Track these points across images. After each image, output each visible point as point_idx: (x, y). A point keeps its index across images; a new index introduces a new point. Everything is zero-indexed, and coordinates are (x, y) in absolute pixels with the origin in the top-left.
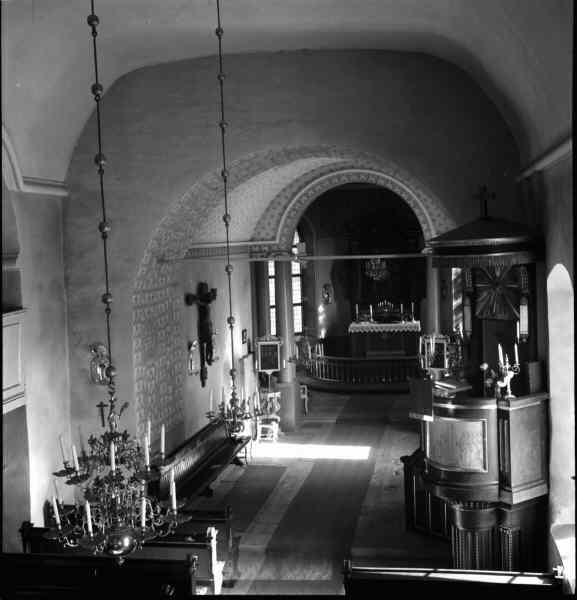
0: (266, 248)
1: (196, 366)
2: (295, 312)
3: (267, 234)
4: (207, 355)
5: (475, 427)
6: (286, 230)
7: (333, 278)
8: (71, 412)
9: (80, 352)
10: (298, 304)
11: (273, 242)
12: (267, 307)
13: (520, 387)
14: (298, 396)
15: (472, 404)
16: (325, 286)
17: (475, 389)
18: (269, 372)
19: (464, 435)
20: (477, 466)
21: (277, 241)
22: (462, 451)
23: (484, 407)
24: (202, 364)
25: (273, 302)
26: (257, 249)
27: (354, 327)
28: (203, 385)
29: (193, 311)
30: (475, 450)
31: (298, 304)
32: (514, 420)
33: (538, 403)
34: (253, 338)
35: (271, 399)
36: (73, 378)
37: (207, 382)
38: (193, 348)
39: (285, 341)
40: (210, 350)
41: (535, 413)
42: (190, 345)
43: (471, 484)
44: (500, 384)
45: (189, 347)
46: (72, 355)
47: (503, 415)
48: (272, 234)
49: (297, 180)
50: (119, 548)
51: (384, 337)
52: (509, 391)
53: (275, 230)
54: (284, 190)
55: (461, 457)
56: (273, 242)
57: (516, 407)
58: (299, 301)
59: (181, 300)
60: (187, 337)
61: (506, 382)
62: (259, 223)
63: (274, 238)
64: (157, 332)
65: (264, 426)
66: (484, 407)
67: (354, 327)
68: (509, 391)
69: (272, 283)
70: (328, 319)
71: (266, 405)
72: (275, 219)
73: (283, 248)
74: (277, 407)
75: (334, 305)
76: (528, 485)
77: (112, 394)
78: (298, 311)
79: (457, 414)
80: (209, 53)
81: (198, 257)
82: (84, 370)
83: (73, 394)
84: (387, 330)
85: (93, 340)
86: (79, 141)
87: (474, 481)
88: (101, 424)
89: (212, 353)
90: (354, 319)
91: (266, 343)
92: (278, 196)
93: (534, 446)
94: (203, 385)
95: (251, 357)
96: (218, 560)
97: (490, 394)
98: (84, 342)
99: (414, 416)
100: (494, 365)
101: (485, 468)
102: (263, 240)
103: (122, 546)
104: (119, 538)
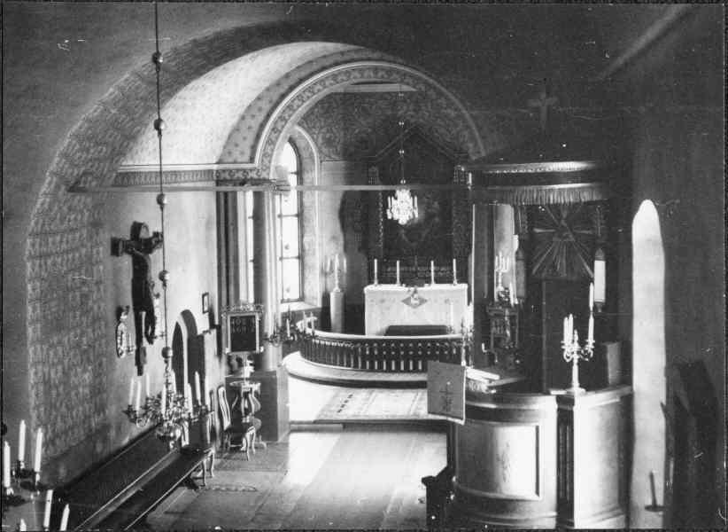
28: (140, 372)
37: (146, 368)
47: (565, 420)
63: (252, 160)
87: (520, 513)
92: (259, 98)
93: (609, 462)
94: (140, 372)
95: (214, 332)
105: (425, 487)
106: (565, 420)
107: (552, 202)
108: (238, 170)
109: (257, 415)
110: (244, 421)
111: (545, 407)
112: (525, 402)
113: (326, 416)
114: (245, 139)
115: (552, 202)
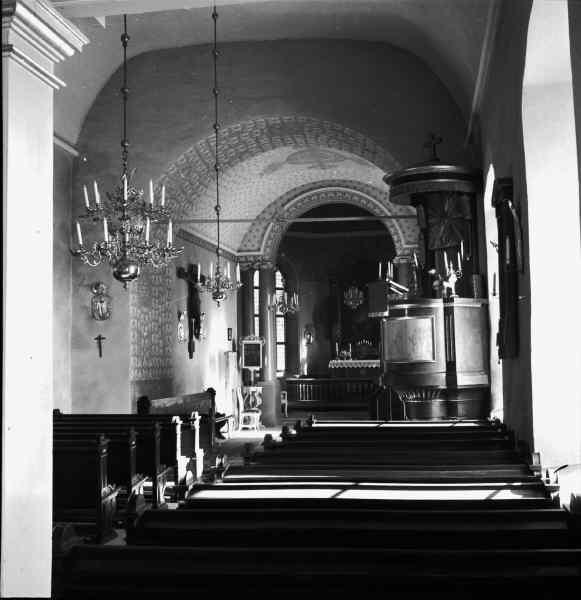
0: (252, 259)
1: (183, 332)
2: (278, 324)
3: (253, 246)
4: (195, 329)
5: (424, 323)
6: (270, 242)
7: (315, 319)
8: (72, 344)
9: (83, 291)
10: (282, 343)
11: (256, 253)
12: (251, 316)
13: (464, 289)
14: (278, 399)
15: (424, 302)
16: (307, 327)
17: (425, 290)
18: (252, 369)
19: (415, 331)
20: (428, 357)
21: (261, 253)
22: (414, 345)
23: (432, 306)
24: (191, 337)
25: (257, 312)
26: (243, 259)
27: (334, 364)
28: (191, 357)
29: (183, 285)
30: (425, 344)
31: (282, 343)
32: (458, 314)
33: (479, 306)
34: (238, 337)
35: (253, 392)
36: (74, 310)
37: (194, 354)
38: (182, 317)
39: (267, 339)
40: (198, 325)
41: (476, 313)
42: (180, 315)
43: (422, 373)
44: (446, 284)
45: (179, 317)
46: (76, 291)
47: (449, 312)
48: (257, 246)
49: (281, 198)
50: (126, 273)
51: (362, 372)
52: (453, 292)
53: (260, 242)
54: (269, 206)
55: (413, 350)
56: (256, 253)
57: (459, 303)
58: (283, 341)
59: (173, 272)
60: (178, 306)
61: (451, 283)
62: (246, 236)
63: (259, 250)
64: (154, 292)
65: (247, 414)
66: (432, 306)
67: (334, 364)
68: (453, 292)
69: (256, 292)
70: (310, 356)
71: (248, 399)
72: (260, 233)
73: (267, 258)
74: (259, 401)
75: (316, 345)
76: (470, 372)
77: (125, 160)
78: (281, 349)
79: (412, 312)
80: (209, 41)
81: (187, 240)
82: (85, 307)
83: (74, 328)
84: (365, 366)
85: (95, 280)
86: (91, 111)
87: (425, 370)
88: (98, 354)
89: (200, 327)
90: (334, 357)
91: (251, 342)
92: (264, 212)
93: (477, 342)
94: (191, 357)
95: (235, 354)
96: (201, 447)
97: (434, 295)
98: (86, 283)
99: (373, 315)
100: (443, 272)
101: (434, 358)
102: (249, 251)
103: (128, 272)
104: (127, 266)
105: (494, 209)
106: (449, 312)
107: (417, 246)
108: (250, 256)
109: (259, 407)
110: (279, 439)
111: (438, 305)
112: (429, 303)
113: (269, 199)
114: (255, 237)
115: (417, 246)
